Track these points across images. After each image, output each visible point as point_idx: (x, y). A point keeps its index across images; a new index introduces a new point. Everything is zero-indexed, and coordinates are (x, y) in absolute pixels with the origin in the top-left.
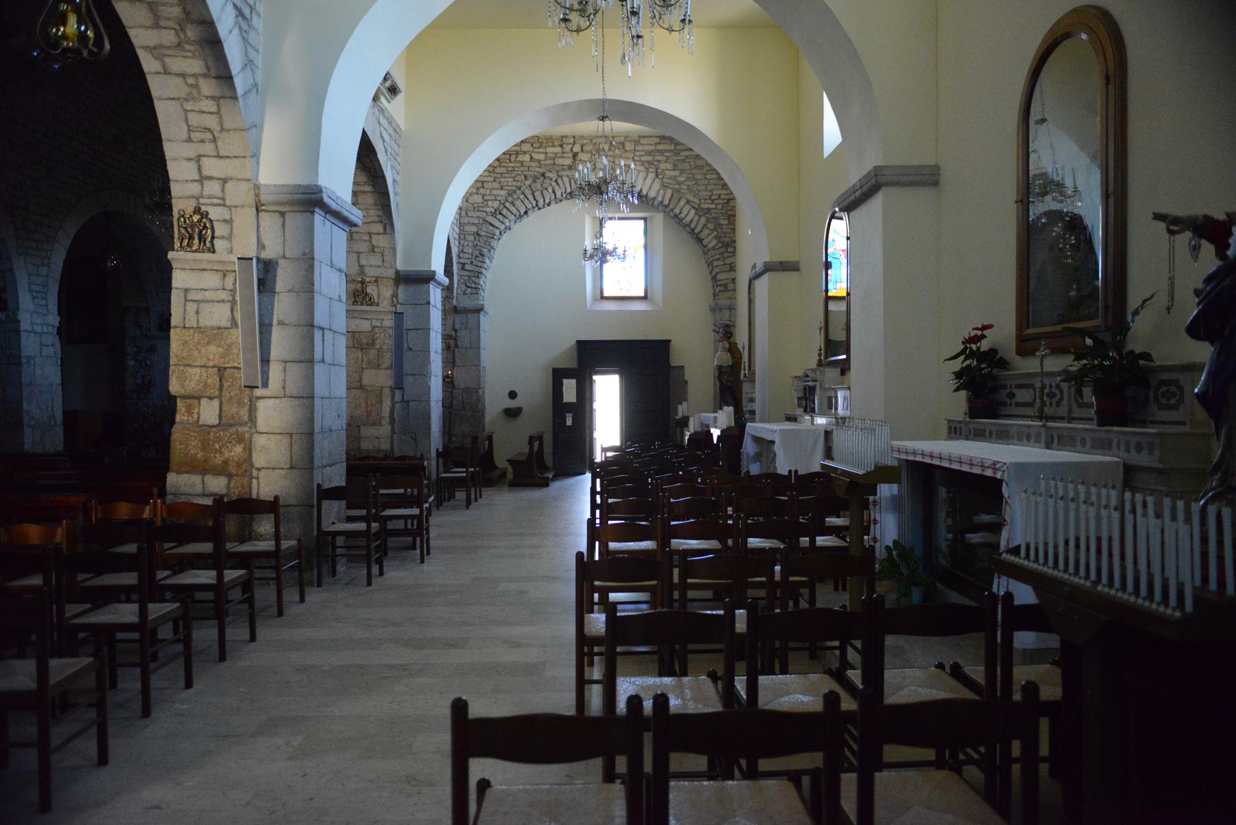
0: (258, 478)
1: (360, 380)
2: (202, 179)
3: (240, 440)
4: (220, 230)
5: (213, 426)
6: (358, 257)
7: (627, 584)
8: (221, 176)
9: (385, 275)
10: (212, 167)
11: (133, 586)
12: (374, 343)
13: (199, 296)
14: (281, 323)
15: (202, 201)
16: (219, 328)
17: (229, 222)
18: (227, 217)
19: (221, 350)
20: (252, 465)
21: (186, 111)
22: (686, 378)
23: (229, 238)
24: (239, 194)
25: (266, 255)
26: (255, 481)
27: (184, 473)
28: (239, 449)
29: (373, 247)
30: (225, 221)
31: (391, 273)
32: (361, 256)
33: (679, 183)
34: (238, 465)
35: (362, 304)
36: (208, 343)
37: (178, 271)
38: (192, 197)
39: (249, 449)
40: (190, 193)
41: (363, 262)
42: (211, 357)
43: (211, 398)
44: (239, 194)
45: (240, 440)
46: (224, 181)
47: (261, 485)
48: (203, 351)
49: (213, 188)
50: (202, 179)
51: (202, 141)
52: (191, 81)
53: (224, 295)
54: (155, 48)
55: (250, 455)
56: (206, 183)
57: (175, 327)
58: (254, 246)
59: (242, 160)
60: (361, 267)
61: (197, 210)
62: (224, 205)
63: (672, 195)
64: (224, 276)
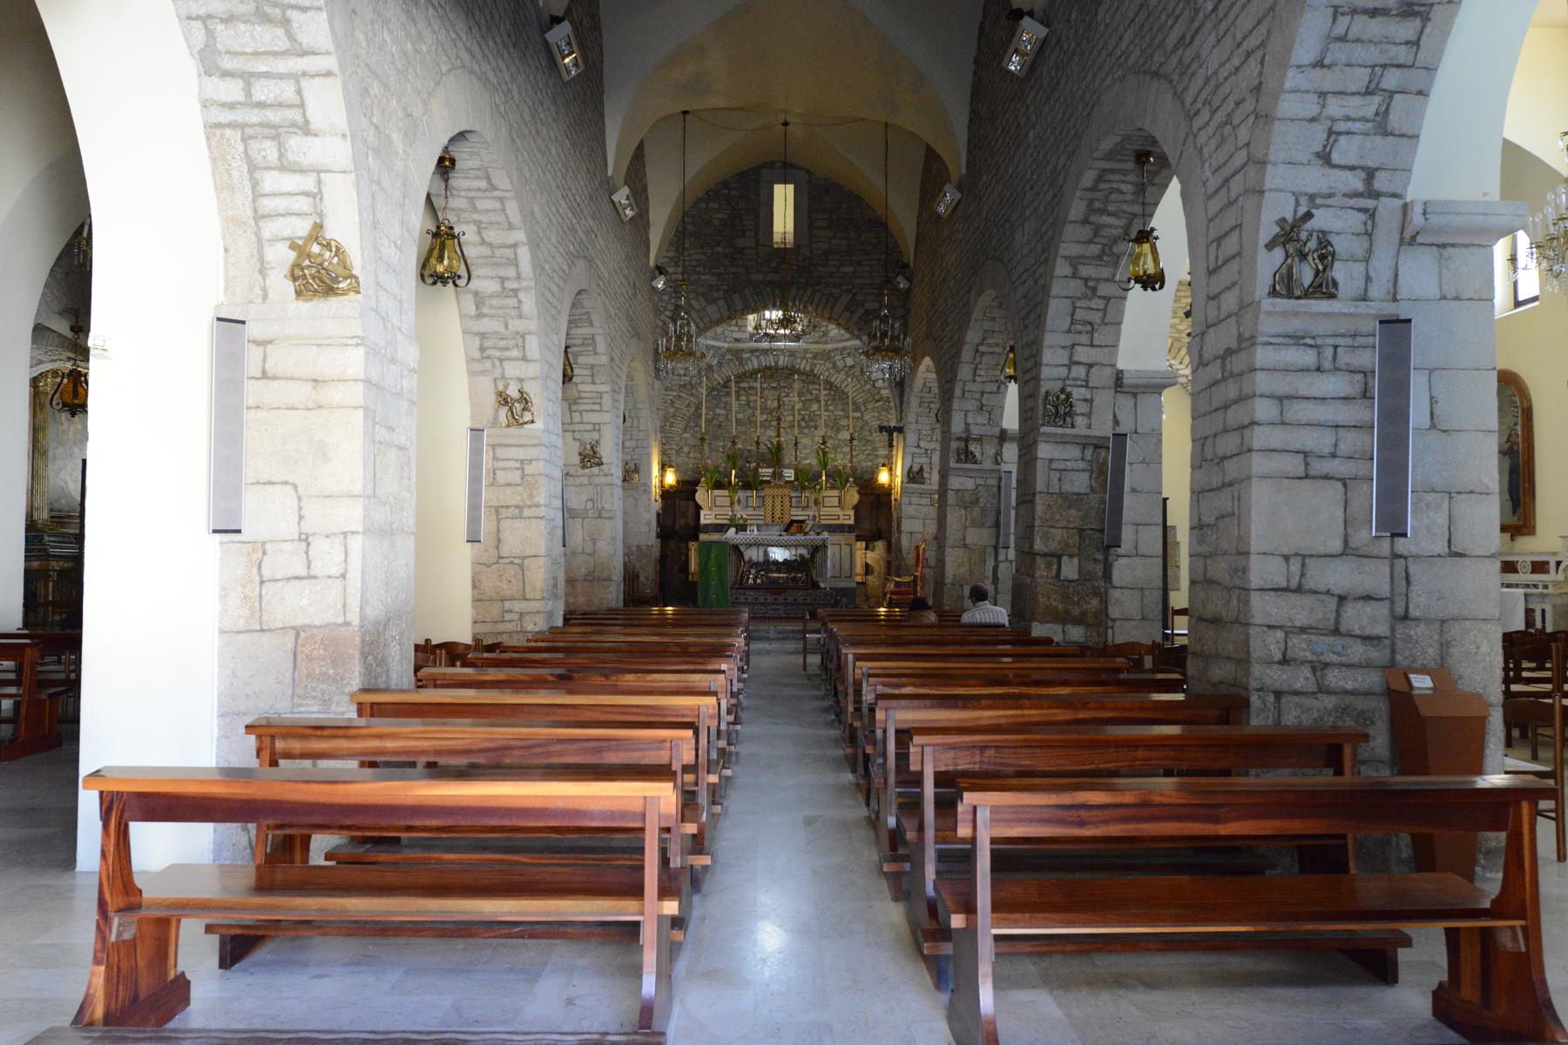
0: (1112, 628)
1: (964, 539)
2: (1072, 363)
3: (1096, 593)
4: (1080, 408)
5: (1073, 581)
6: (966, 415)
7: (910, 790)
8: (1089, 362)
9: (989, 433)
10: (1083, 354)
11: (1513, 683)
12: (977, 501)
13: (1061, 466)
14: (1133, 490)
15: (1068, 382)
16: (1079, 494)
17: (1090, 401)
18: (1089, 397)
19: (1080, 513)
20: (1107, 615)
21: (1075, 307)
22: (1178, 540)
23: (1089, 415)
24: (1101, 377)
25: (1119, 430)
26: (1110, 631)
27: (1047, 622)
28: (1095, 602)
29: (982, 405)
30: (1086, 400)
31: (996, 431)
32: (969, 414)
33: (1179, 331)
34: (1096, 615)
35: (966, 462)
36: (1069, 508)
37: (1043, 444)
38: (1059, 379)
39: (1105, 601)
40: (1057, 376)
41: (970, 420)
42: (1071, 519)
43: (1071, 556)
44: (1101, 377)
45: (1096, 593)
46: (1091, 366)
47: (1116, 635)
48: (1064, 514)
49: (1079, 372)
50: (1072, 363)
51: (1080, 332)
52: (1091, 284)
53: (1082, 465)
54: (1075, 258)
55: (1106, 608)
56: (1075, 368)
57: (1040, 493)
58: (1110, 423)
59: (1111, 348)
60: (967, 424)
61: (1063, 390)
62: (1087, 386)
63: (1172, 344)
64: (1084, 448)
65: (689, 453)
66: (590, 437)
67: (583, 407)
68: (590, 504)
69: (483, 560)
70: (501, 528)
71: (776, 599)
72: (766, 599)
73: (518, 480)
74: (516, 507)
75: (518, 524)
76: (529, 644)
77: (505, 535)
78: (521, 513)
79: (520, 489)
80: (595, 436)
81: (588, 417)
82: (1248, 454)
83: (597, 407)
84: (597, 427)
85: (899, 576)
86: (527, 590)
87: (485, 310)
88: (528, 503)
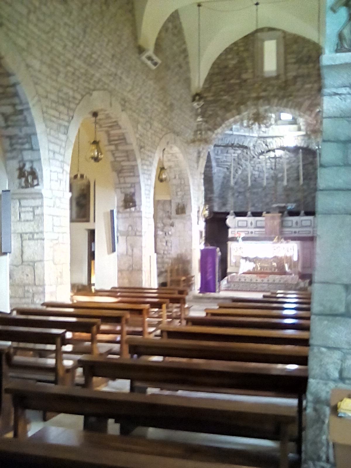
65: (238, 196)
66: (129, 191)
67: (125, 174)
68: (130, 228)
69: (15, 263)
70: (24, 245)
71: (262, 280)
72: (257, 280)
73: (32, 218)
74: (31, 233)
75: (32, 243)
76: (44, 308)
77: (26, 249)
78: (33, 236)
79: (33, 223)
80: (132, 190)
81: (128, 180)
82: (42, 119)
83: (132, 174)
84: (133, 185)
85: (189, 283)
86: (36, 280)
87: (10, 123)
88: (37, 231)
